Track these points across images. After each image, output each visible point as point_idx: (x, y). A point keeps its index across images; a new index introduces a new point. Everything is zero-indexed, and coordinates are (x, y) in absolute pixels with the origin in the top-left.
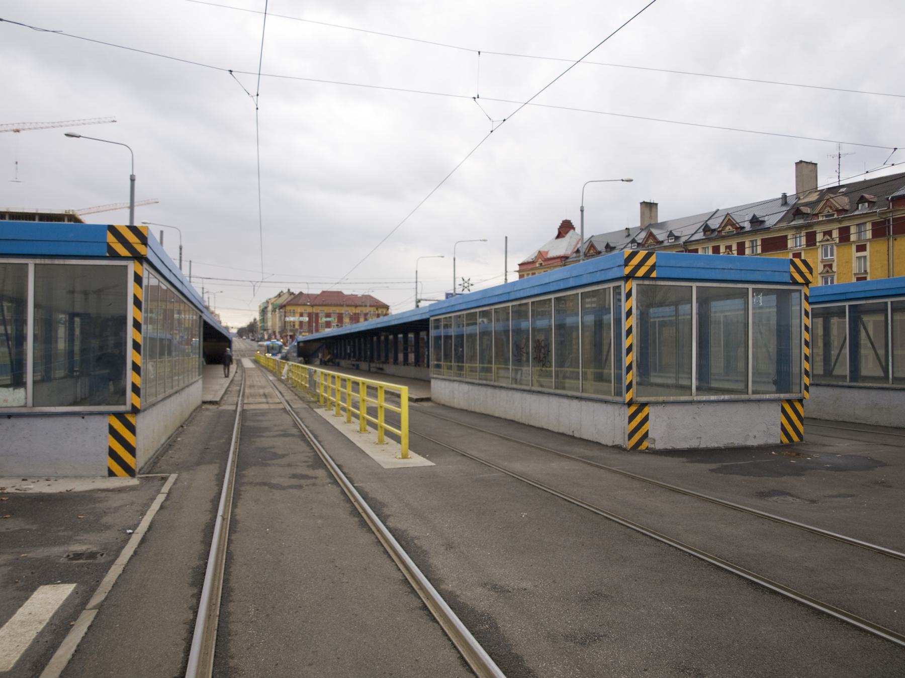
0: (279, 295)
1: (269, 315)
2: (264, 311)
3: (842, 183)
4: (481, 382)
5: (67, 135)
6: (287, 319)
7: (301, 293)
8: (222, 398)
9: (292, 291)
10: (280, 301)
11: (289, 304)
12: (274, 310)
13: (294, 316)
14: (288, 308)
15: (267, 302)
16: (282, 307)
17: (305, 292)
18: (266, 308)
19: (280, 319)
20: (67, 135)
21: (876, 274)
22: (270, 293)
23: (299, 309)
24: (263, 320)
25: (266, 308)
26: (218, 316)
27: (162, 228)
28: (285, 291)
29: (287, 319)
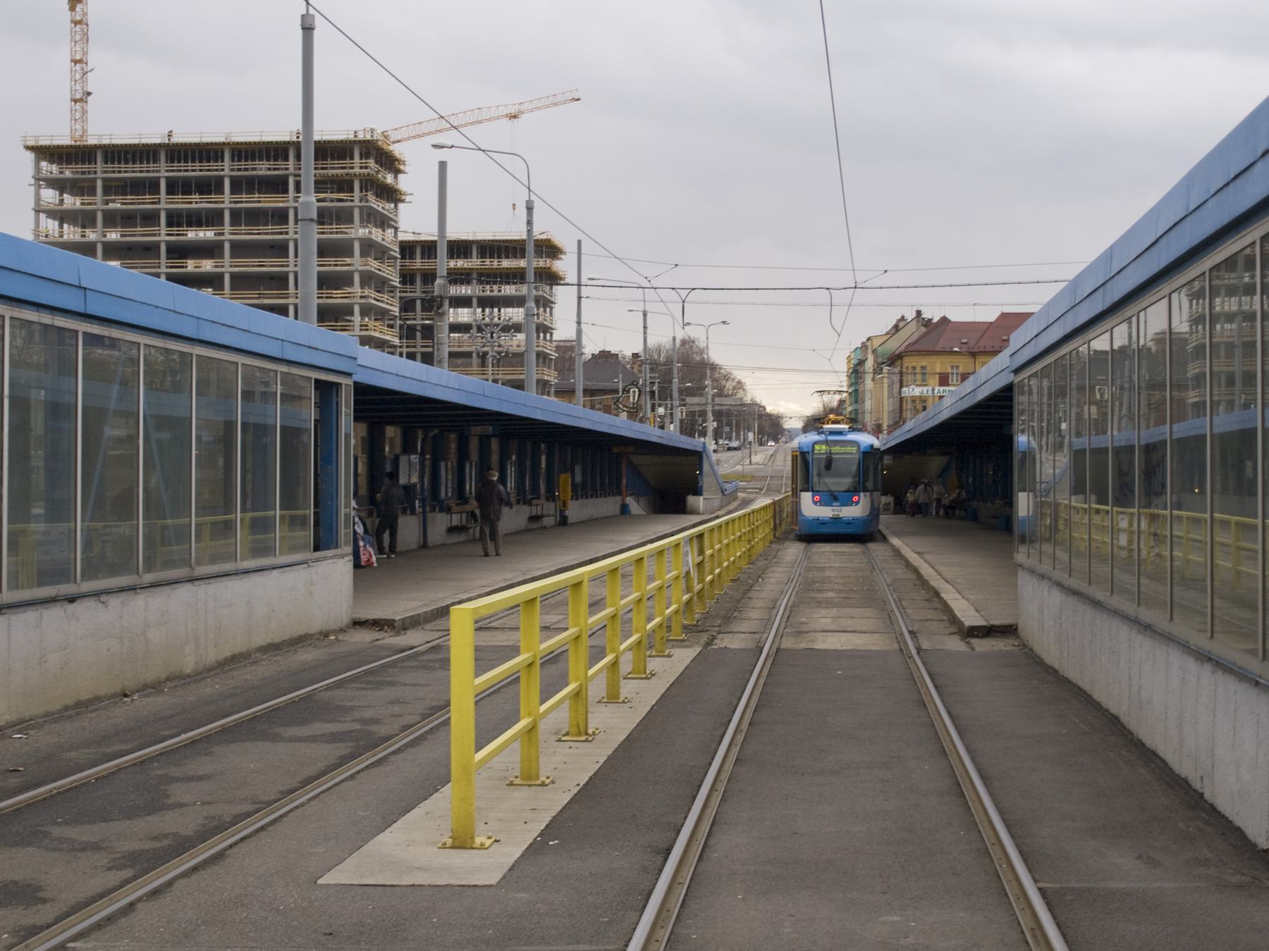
0: (896, 328)
1: (869, 383)
2: (856, 373)
3: (456, 231)
4: (116, 333)
5: (434, 146)
6: (908, 392)
7: (944, 320)
8: (769, 556)
9: (926, 315)
10: (895, 345)
11: (913, 350)
12: (878, 370)
13: (924, 383)
14: (909, 362)
15: (864, 346)
16: (895, 359)
17: (954, 317)
18: (861, 363)
19: (890, 395)
20: (434, 146)
21: (514, 292)
22: (873, 322)
23: (938, 365)
24: (856, 394)
25: (861, 363)
26: (740, 385)
27: (582, 237)
28: (910, 315)
29: (908, 392)
